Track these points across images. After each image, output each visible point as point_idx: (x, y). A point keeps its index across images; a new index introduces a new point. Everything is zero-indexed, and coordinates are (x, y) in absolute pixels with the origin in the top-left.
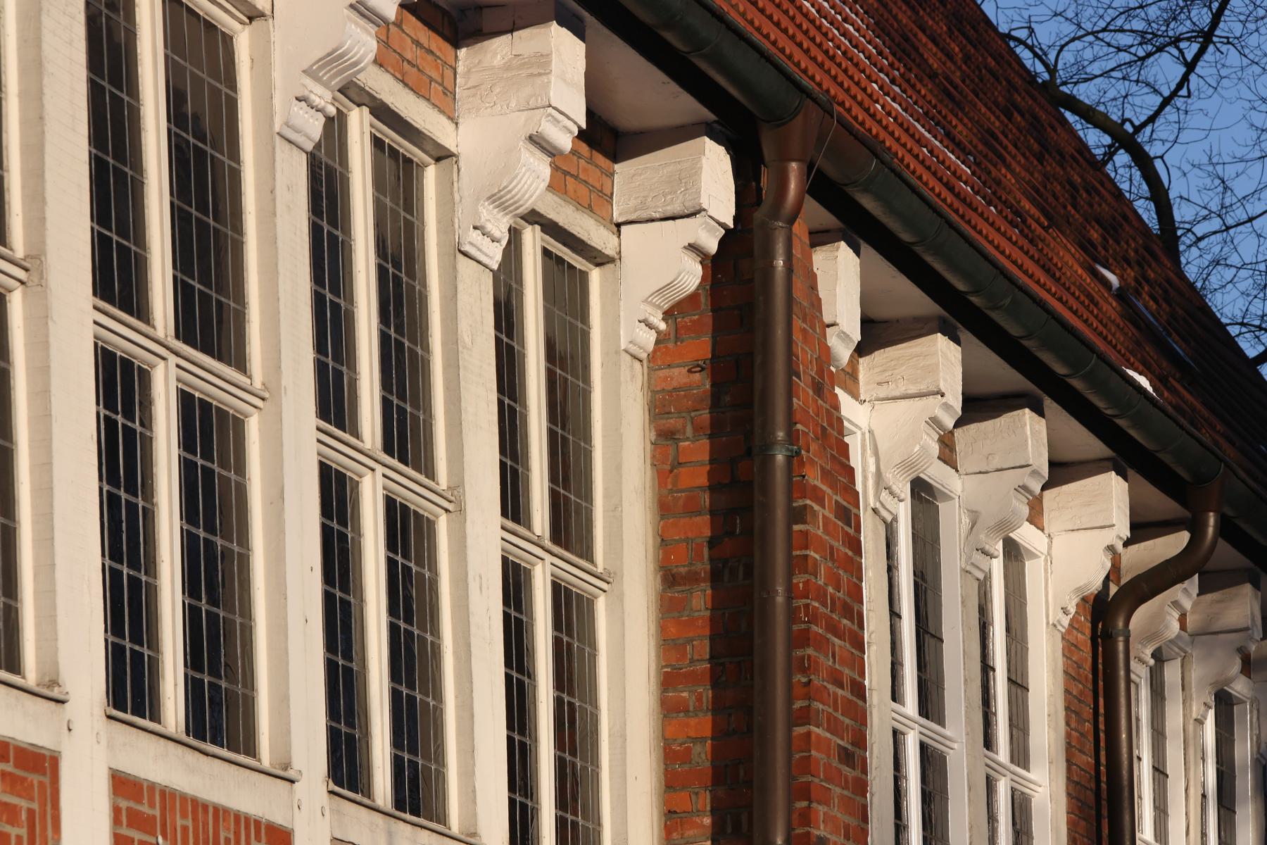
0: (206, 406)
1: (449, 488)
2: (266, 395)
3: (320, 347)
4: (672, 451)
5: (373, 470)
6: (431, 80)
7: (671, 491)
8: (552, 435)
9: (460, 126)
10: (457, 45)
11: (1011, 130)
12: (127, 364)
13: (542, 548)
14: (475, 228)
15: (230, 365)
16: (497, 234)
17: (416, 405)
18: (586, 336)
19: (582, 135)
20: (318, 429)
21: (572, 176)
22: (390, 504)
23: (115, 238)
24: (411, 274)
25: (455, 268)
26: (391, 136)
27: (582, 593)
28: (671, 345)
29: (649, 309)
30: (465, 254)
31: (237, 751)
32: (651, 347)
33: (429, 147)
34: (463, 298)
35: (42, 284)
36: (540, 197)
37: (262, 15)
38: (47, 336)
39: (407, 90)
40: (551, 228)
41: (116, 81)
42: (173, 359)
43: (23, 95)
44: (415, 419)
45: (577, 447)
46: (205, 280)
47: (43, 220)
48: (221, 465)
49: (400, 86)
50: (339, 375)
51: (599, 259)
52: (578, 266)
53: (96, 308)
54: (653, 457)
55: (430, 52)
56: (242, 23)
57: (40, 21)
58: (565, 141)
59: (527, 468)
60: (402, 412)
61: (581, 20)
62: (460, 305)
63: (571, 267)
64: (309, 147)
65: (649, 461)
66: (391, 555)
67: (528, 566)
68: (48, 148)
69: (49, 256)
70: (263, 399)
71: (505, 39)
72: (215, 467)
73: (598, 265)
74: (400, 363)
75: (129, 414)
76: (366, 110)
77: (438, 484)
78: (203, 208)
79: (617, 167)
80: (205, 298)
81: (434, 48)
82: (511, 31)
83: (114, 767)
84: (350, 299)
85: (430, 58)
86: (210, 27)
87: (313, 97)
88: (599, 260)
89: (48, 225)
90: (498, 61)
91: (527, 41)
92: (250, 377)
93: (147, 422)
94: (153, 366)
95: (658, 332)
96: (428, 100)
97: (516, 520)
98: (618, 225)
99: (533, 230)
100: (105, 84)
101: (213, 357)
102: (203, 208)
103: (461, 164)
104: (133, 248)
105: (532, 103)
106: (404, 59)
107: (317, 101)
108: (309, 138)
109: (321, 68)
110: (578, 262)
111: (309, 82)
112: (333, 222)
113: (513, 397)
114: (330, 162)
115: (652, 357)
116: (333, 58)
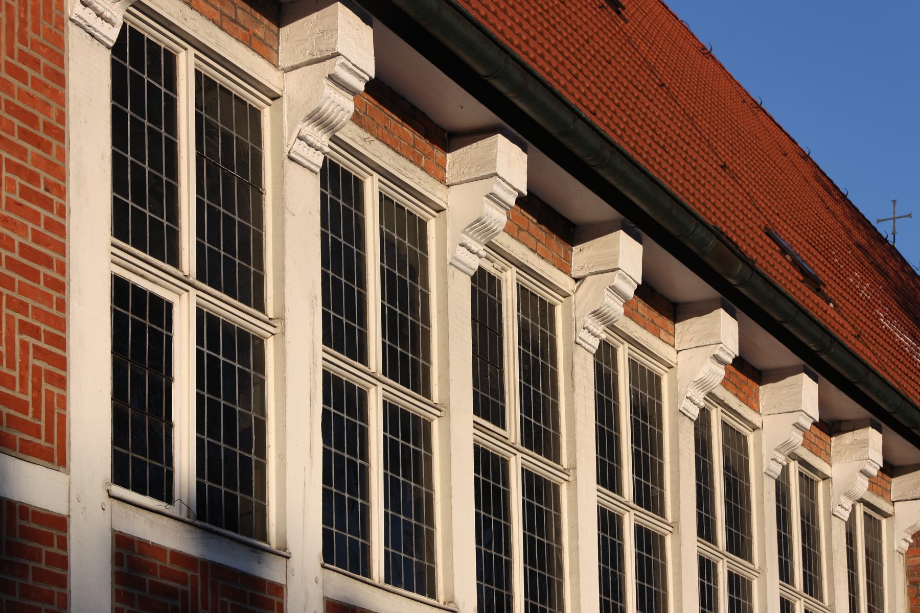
0: (737, 576)
1: (829, 605)
2: (760, 571)
3: (780, 552)
4: (916, 590)
5: (800, 599)
6: (821, 449)
7: (916, 605)
8: (868, 584)
9: (833, 467)
10: (831, 436)
11: (894, 308)
12: (708, 561)
13: (724, 555)
14: (839, 505)
15: (746, 560)
16: (847, 508)
17: (816, 574)
18: (881, 545)
19: (881, 470)
20: (780, 584)
21: (875, 484)
22: (730, 574)
23: (704, 514)
24: (814, 523)
25: (831, 521)
26: (806, 471)
27: (605, 507)
28: (915, 548)
29: (906, 534)
30: (835, 515)
31: (423, 594)
32: (907, 549)
33: (820, 474)
34: (834, 532)
35: (679, 532)
36: (864, 493)
37: (758, 428)
38: (680, 552)
39: (812, 454)
40: (867, 504)
41: (704, 455)
42: (726, 559)
43: (672, 462)
44: (815, 579)
45: (878, 589)
46: (737, 528)
47: (679, 508)
48: (743, 599)
49: (810, 452)
50: (786, 563)
51: (886, 515)
52: (877, 518)
53: (698, 541)
54: (908, 592)
55: (821, 439)
56: (750, 431)
57: (678, 435)
58: (874, 472)
59: (859, 597)
60: (811, 576)
61: (880, 426)
62: (833, 535)
63: (874, 518)
64: (776, 477)
65: (906, 593)
66: (169, 334)
67: (793, 602)
68: (681, 482)
69: (681, 522)
70: (759, 573)
71: (850, 434)
72: (741, 599)
73: (885, 517)
74: (810, 557)
75: (709, 580)
76: (796, 462)
77: (370, 368)
78: (736, 501)
79: (893, 480)
80: (737, 535)
81: (822, 437)
82: (853, 431)
83: (326, 595)
84: (791, 533)
85: (821, 441)
86: (738, 433)
87: (778, 459)
88: (886, 516)
89: (681, 511)
90: (848, 442)
91: (859, 434)
92: (754, 565)
93: (716, 583)
94: (718, 562)
95: (910, 543)
96: (820, 457)
97: (787, 582)
98: (893, 502)
99: (860, 505)
100: (700, 456)
101: (740, 557)
102: (736, 501)
103: (833, 481)
104: (711, 517)
105: (861, 458)
106: (811, 442)
107: (780, 460)
108: (776, 473)
109: (781, 448)
110: (877, 516)
111: (776, 453)
112: (784, 505)
113: (853, 570)
114: (783, 482)
115: (907, 553)
116: (786, 444)
